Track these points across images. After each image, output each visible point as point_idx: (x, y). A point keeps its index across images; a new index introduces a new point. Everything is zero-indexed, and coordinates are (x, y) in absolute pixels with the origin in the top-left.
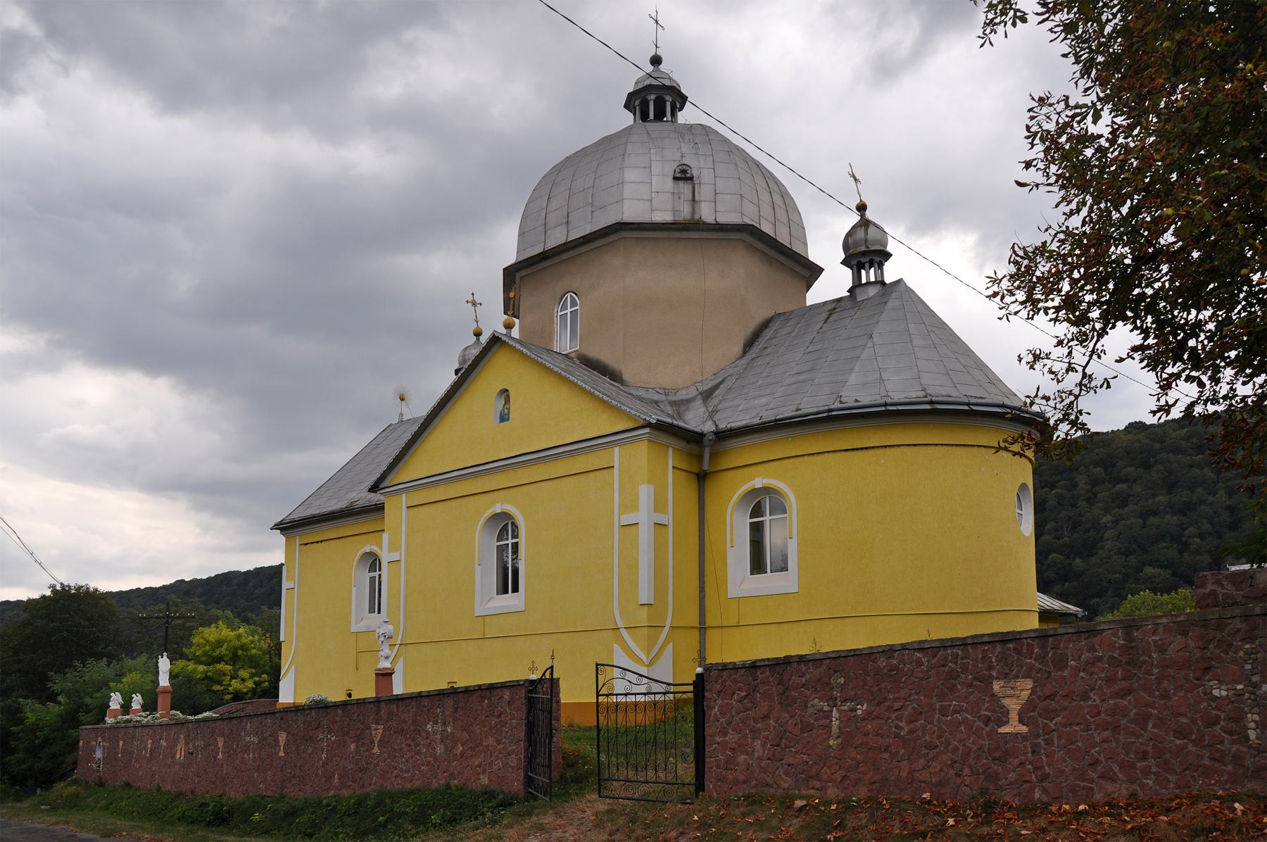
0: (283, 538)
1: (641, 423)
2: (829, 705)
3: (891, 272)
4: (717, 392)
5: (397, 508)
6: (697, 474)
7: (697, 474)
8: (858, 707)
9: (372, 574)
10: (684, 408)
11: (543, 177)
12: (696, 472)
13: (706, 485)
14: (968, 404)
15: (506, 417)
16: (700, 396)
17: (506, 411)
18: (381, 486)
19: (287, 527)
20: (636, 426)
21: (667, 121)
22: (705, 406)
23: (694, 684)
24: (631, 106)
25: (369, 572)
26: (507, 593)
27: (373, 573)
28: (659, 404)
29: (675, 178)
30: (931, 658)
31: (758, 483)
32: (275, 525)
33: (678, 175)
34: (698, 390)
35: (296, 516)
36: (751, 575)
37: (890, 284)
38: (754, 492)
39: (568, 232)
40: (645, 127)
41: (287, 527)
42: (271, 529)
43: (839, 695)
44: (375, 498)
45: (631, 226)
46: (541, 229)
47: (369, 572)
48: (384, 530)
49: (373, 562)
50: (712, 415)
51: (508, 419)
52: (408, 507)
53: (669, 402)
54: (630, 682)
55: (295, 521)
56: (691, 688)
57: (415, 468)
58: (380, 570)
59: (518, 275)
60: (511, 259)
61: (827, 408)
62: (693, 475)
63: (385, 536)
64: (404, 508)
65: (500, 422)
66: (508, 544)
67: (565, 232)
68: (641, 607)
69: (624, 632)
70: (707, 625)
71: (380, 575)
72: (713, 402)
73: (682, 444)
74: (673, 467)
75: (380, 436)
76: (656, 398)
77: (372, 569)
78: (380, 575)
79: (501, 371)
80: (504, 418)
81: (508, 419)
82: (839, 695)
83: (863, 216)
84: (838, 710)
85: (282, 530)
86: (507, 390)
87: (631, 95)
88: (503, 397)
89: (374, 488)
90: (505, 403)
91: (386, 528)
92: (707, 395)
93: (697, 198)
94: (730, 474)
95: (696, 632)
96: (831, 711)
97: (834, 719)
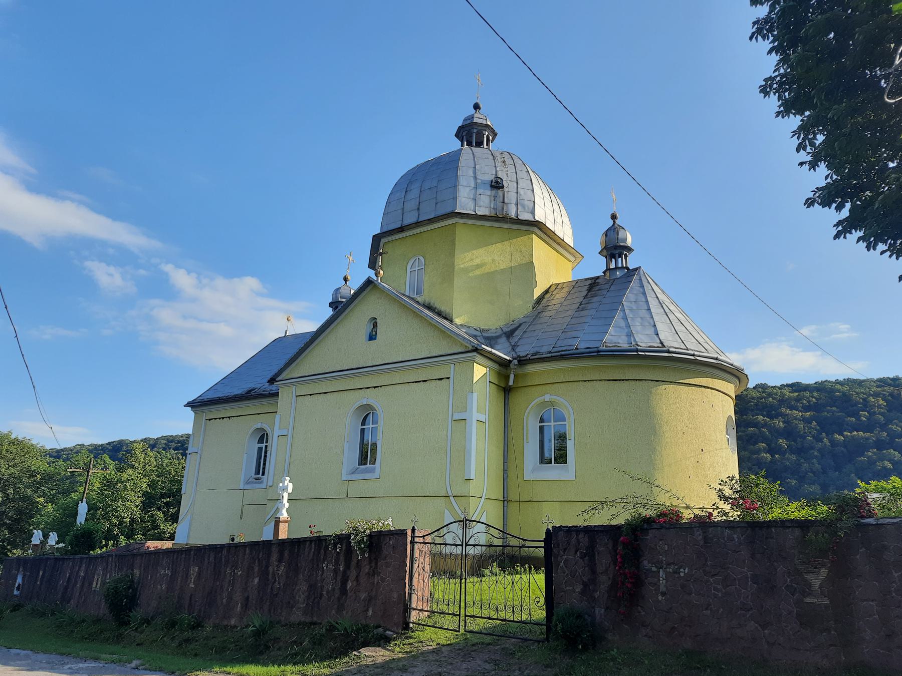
0: (193, 414)
1: (471, 348)
2: (656, 567)
3: (632, 262)
4: (517, 333)
5: (287, 395)
6: (504, 388)
7: (504, 388)
8: (682, 570)
9: (260, 445)
10: (494, 342)
11: (402, 177)
12: (503, 386)
13: (510, 397)
14: (693, 355)
15: (374, 337)
16: (504, 335)
17: (374, 333)
18: (277, 379)
19: (196, 405)
20: (463, 350)
21: (483, 148)
22: (509, 341)
23: (545, 540)
24: (460, 136)
25: (258, 443)
26: (366, 464)
27: (261, 444)
28: (478, 338)
29: (491, 186)
30: (740, 535)
31: (547, 398)
32: (187, 404)
33: (493, 184)
34: (502, 330)
35: (206, 398)
36: (540, 464)
37: (632, 269)
38: (544, 403)
39: (419, 215)
40: (472, 150)
41: (196, 405)
42: (185, 406)
43: (664, 559)
44: (273, 388)
45: (462, 215)
46: (400, 211)
47: (258, 443)
48: (277, 412)
49: (263, 437)
50: (514, 348)
51: (375, 339)
52: (297, 396)
53: (483, 337)
54: (493, 536)
55: (204, 401)
56: (542, 544)
57: (306, 367)
58: (267, 442)
59: (383, 241)
60: (378, 231)
61: (596, 349)
62: (502, 388)
63: (277, 416)
64: (294, 397)
65: (369, 341)
66: (369, 428)
67: (417, 215)
68: (466, 481)
69: (452, 498)
70: (510, 498)
71: (266, 447)
72: (514, 340)
73: (496, 366)
74: (490, 382)
75: (271, 344)
76: (475, 334)
77: (261, 440)
78: (266, 447)
79: (370, 307)
80: (372, 337)
81: (375, 339)
82: (664, 559)
83: (614, 222)
84: (663, 571)
85: (192, 407)
86: (376, 318)
87: (460, 128)
88: (372, 323)
89: (272, 381)
90: (374, 327)
91: (278, 411)
92: (509, 335)
93: (506, 201)
94: (533, 389)
95: (502, 502)
96: (659, 572)
97: (661, 579)
